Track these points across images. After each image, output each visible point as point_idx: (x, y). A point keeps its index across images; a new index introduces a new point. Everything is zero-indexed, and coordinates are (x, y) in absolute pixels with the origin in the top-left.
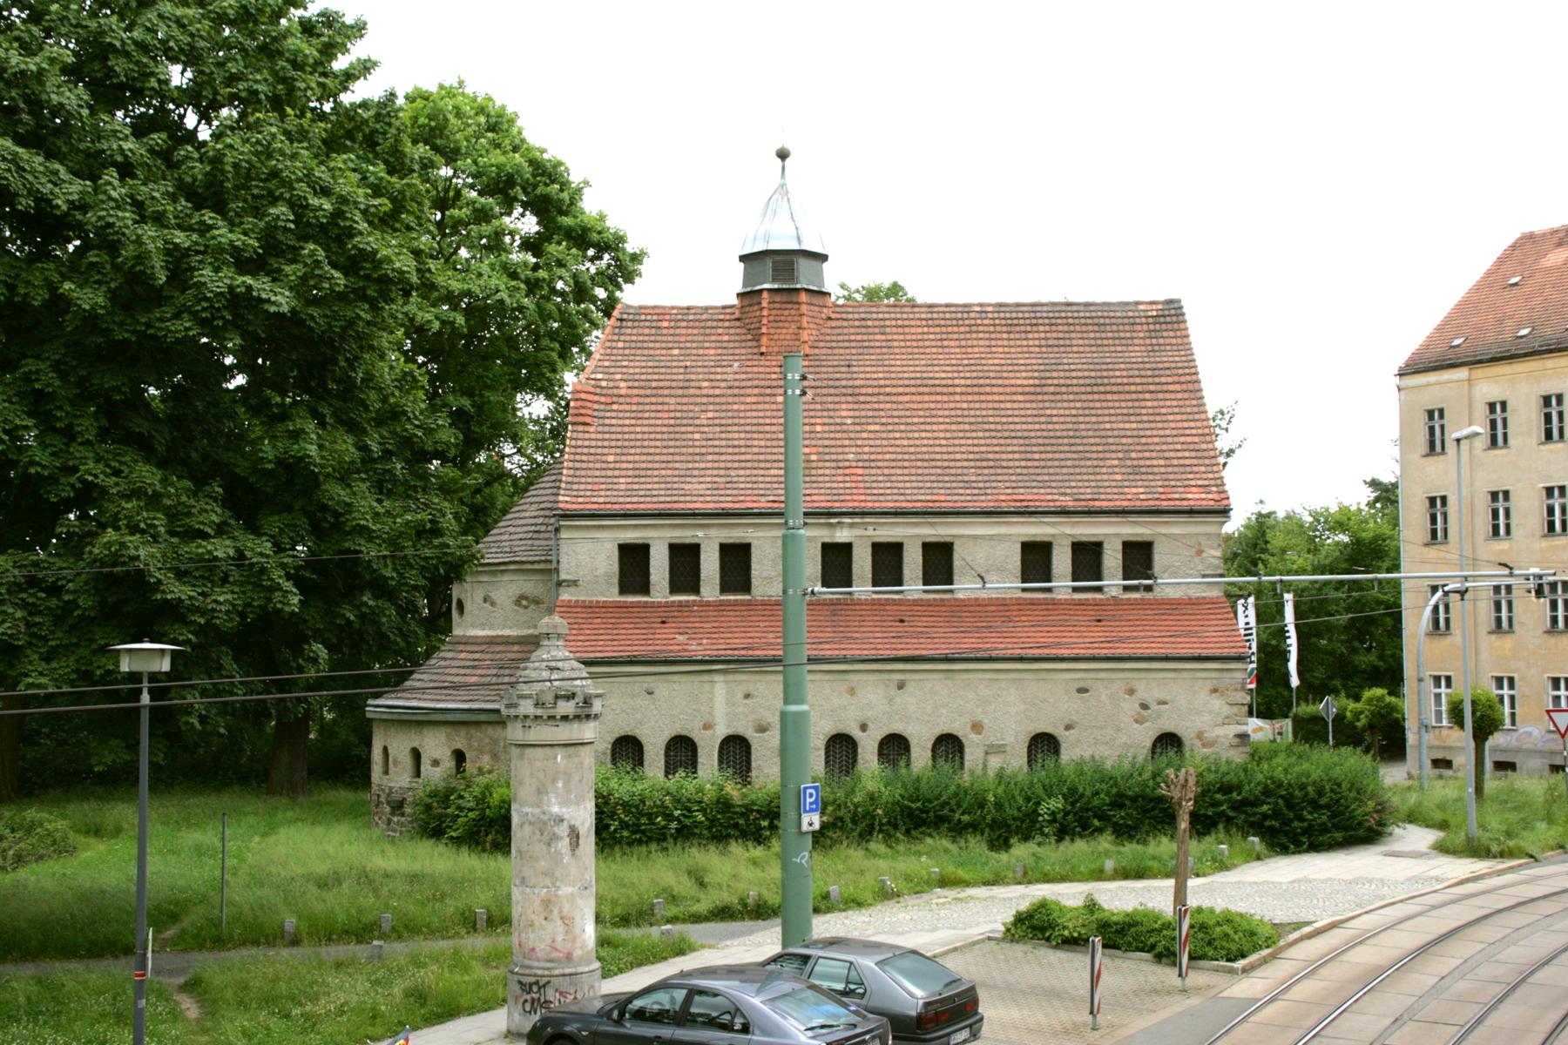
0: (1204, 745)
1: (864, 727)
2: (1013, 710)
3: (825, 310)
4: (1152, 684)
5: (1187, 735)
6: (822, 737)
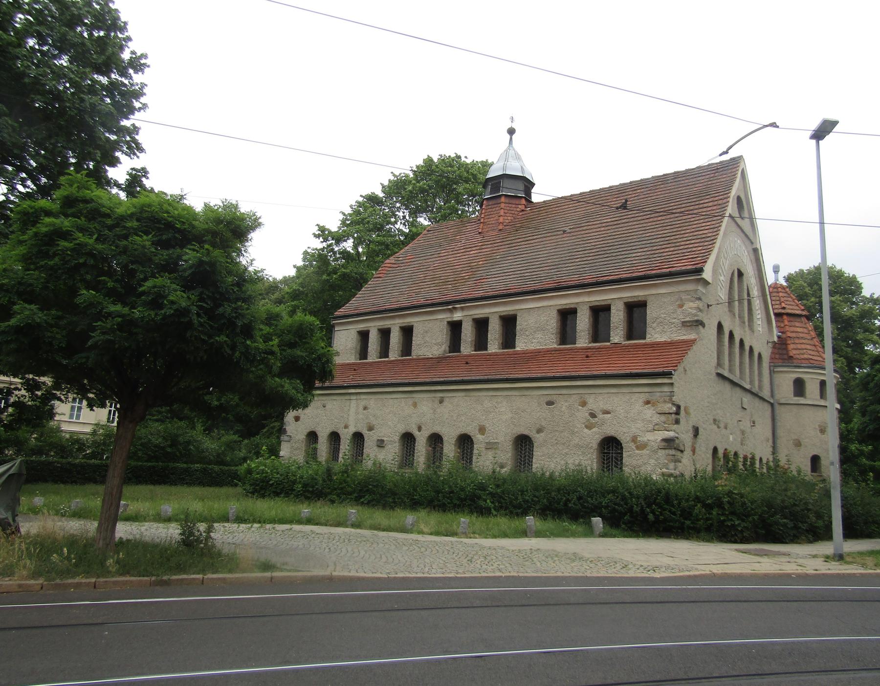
0: (638, 448)
1: (420, 429)
2: (504, 417)
3: (520, 206)
4: (598, 400)
5: (624, 439)
6: (397, 434)
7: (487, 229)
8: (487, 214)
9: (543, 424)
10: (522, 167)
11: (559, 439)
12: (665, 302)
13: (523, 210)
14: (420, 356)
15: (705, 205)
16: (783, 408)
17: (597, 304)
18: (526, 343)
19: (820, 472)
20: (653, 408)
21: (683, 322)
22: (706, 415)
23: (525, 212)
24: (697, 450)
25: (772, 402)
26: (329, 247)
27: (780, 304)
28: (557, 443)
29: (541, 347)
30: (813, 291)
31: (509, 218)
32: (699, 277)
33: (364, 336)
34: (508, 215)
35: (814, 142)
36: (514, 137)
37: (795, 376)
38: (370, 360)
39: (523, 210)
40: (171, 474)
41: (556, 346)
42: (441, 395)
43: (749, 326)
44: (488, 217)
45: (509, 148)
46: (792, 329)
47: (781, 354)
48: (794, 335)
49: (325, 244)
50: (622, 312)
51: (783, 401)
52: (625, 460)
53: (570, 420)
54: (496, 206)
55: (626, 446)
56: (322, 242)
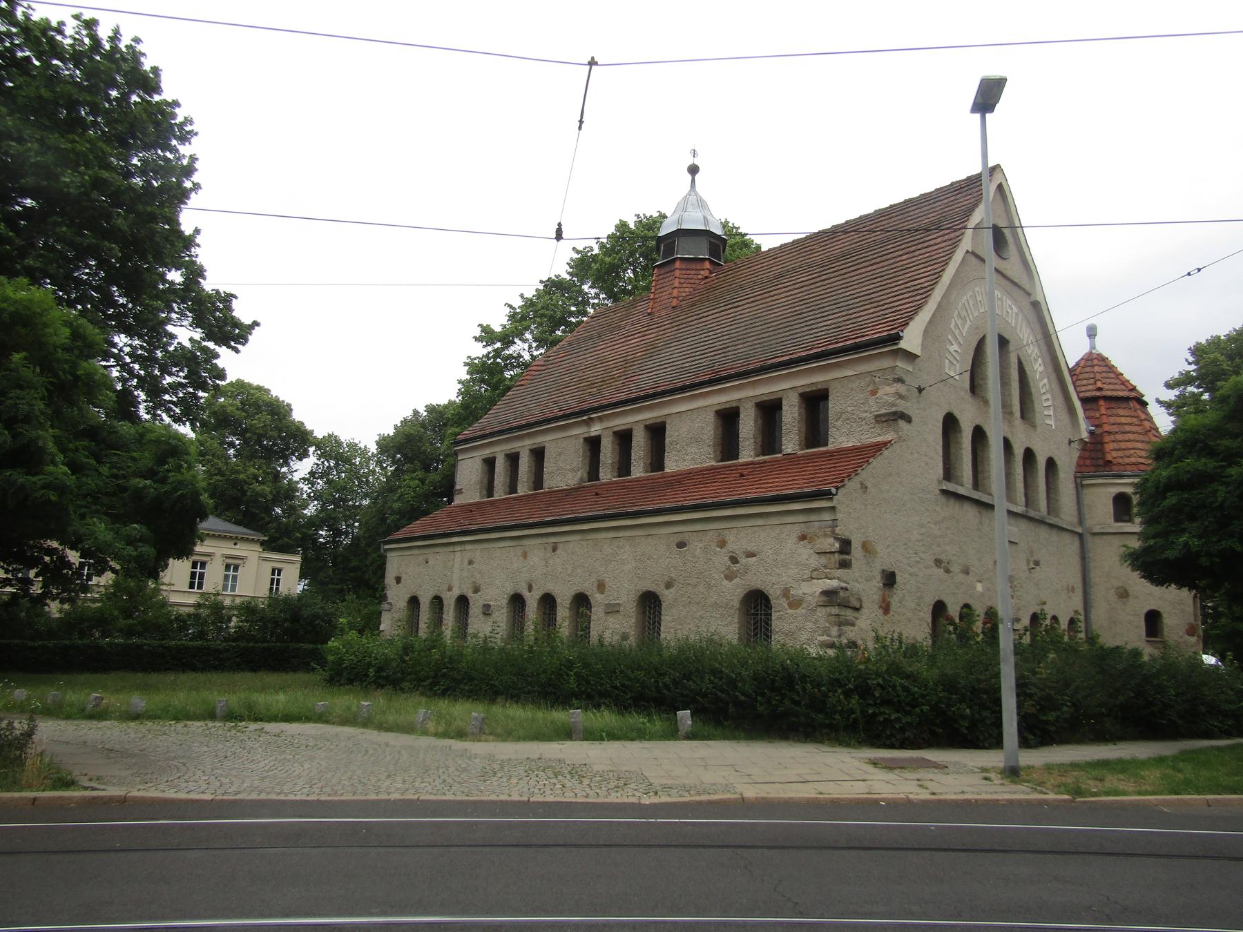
0: (791, 606)
1: (530, 588)
3: (702, 272)
5: (773, 592)
6: (505, 596)
7: (658, 308)
8: (658, 287)
9: (672, 575)
10: (705, 218)
11: (692, 596)
12: (852, 389)
13: (706, 278)
14: (552, 487)
15: (932, 242)
16: (1098, 541)
17: (765, 398)
18: (676, 461)
19: (1163, 638)
20: (810, 546)
21: (876, 416)
22: (916, 553)
23: (709, 280)
24: (894, 606)
25: (1081, 532)
26: (497, 353)
27: (1095, 383)
28: (690, 602)
29: (696, 466)
30: (1234, 367)
31: (687, 290)
32: (895, 347)
33: (490, 463)
34: (685, 285)
35: (977, 116)
36: (697, 177)
37: (1115, 490)
38: (496, 497)
39: (706, 278)
40: (293, 657)
41: (714, 463)
42: (553, 540)
43: (1023, 417)
44: (659, 291)
45: (689, 194)
46: (1112, 420)
47: (1093, 458)
48: (1115, 429)
49: (490, 349)
50: (797, 408)
51: (1097, 529)
52: (776, 624)
53: (705, 567)
54: (669, 275)
55: (776, 603)
56: (485, 346)
